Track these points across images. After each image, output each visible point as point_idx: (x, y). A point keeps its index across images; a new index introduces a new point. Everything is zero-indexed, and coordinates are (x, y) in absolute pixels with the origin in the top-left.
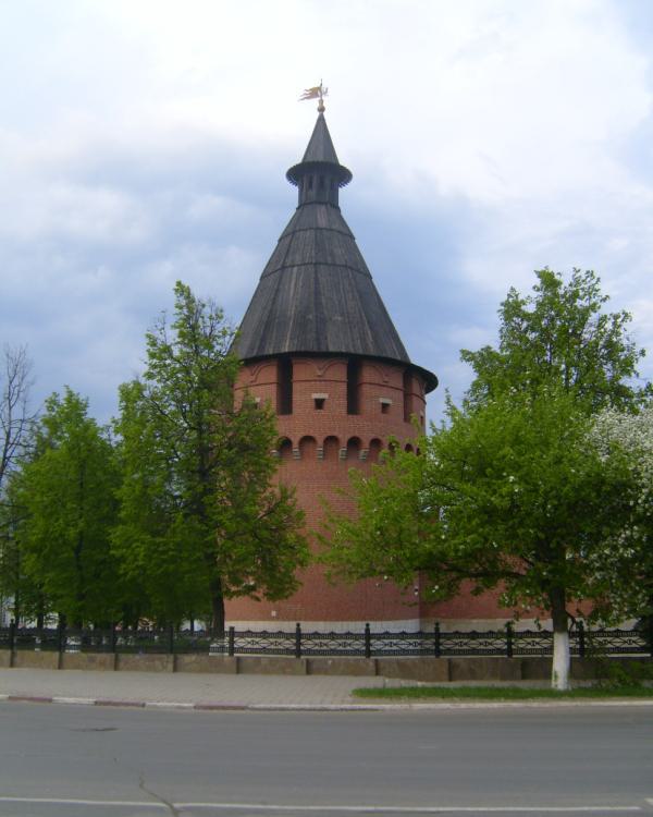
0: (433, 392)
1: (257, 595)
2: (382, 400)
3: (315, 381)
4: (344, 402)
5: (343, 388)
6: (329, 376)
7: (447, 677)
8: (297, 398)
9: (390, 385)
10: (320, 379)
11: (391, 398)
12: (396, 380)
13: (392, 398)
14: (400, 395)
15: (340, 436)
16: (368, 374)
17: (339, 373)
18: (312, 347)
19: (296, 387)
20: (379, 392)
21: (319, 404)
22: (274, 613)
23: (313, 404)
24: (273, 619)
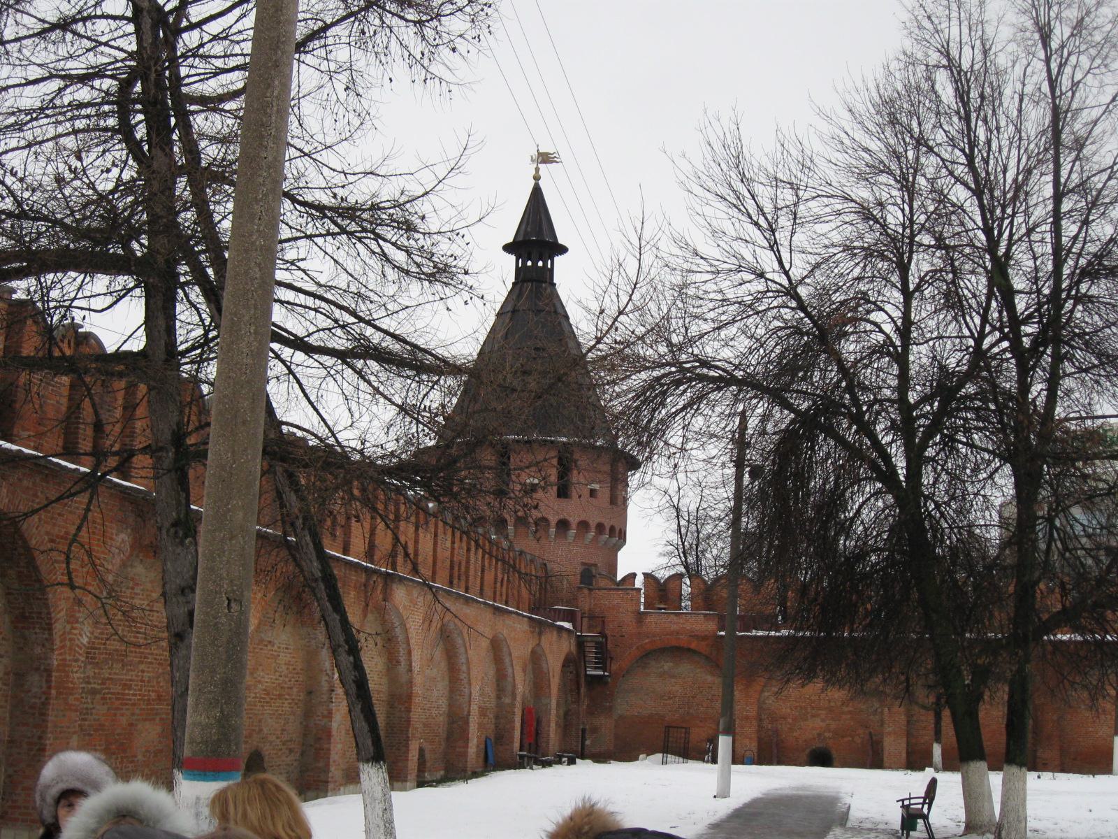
21: (593, 493)
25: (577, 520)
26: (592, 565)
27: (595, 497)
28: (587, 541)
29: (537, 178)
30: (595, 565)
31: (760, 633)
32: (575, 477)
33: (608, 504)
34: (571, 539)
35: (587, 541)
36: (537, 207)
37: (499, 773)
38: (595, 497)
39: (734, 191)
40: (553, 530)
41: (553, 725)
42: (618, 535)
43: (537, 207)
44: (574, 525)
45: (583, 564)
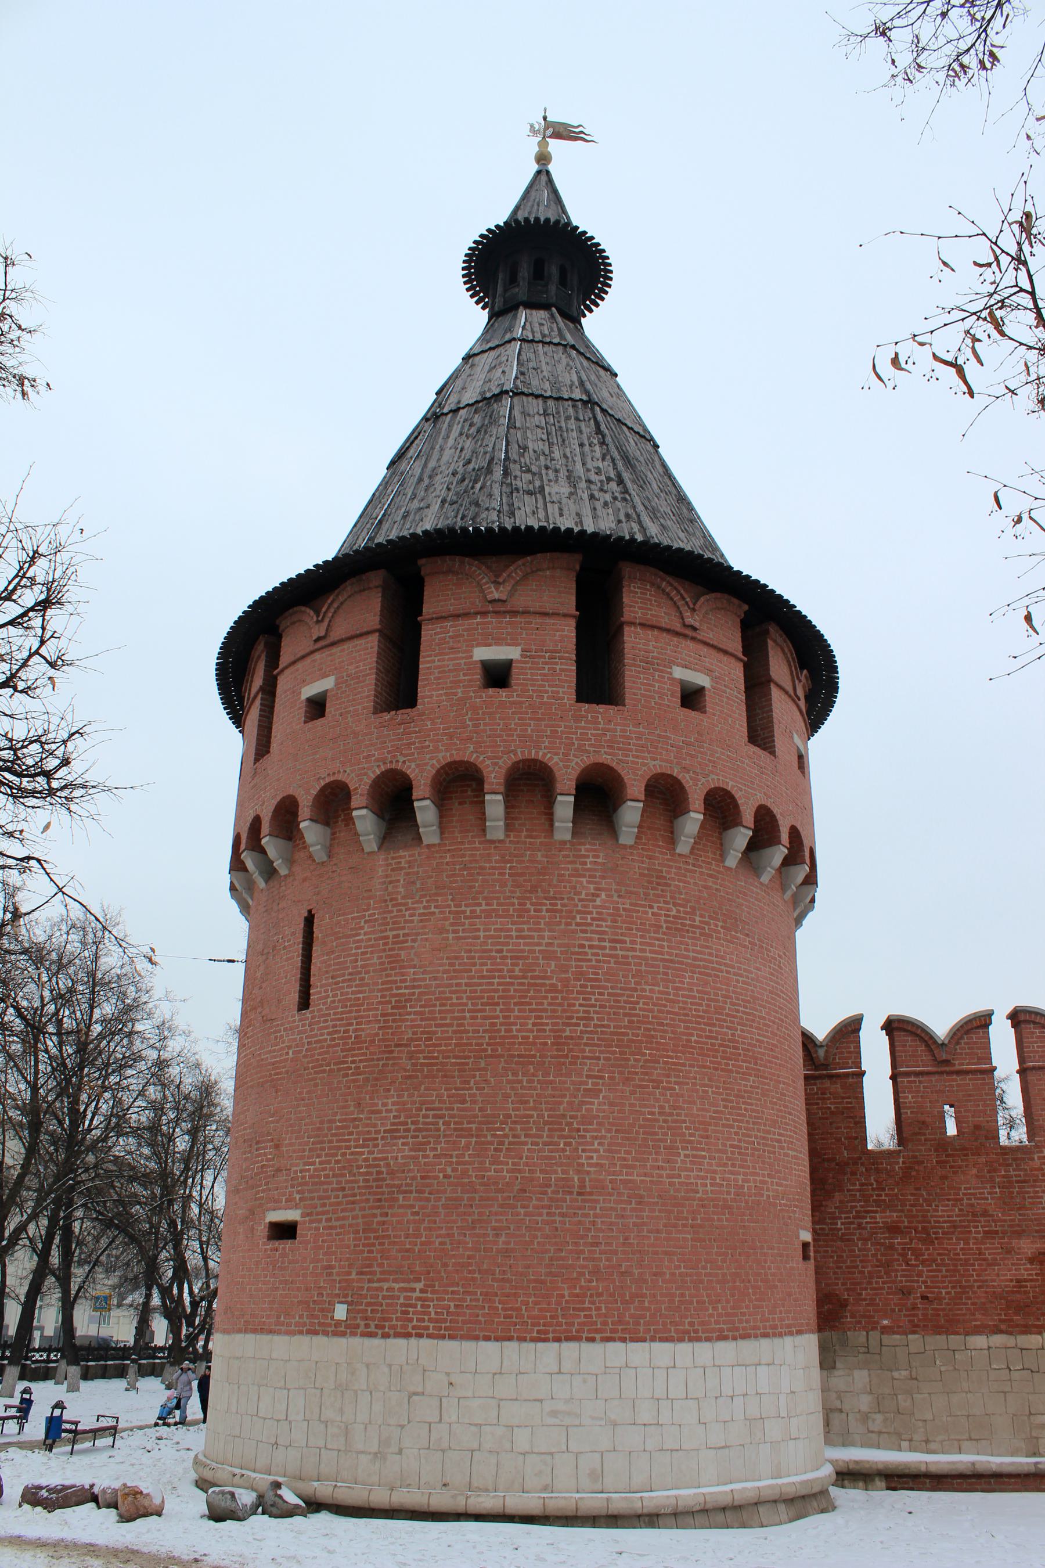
0: (216, 649)
1: (583, 428)
2: (484, 653)
3: (484, 614)
4: (567, 669)
5: (566, 633)
6: (525, 598)
7: (800, 1286)
8: (429, 662)
9: (701, 635)
10: (499, 609)
11: (709, 672)
12: (723, 628)
13: (720, 676)
14: (736, 672)
15: (554, 761)
16: (640, 601)
17: (555, 593)
18: (719, 1451)
19: (429, 634)
20: (673, 655)
21: (497, 676)
22: (341, 1312)
23: (478, 676)
24: (339, 1330)
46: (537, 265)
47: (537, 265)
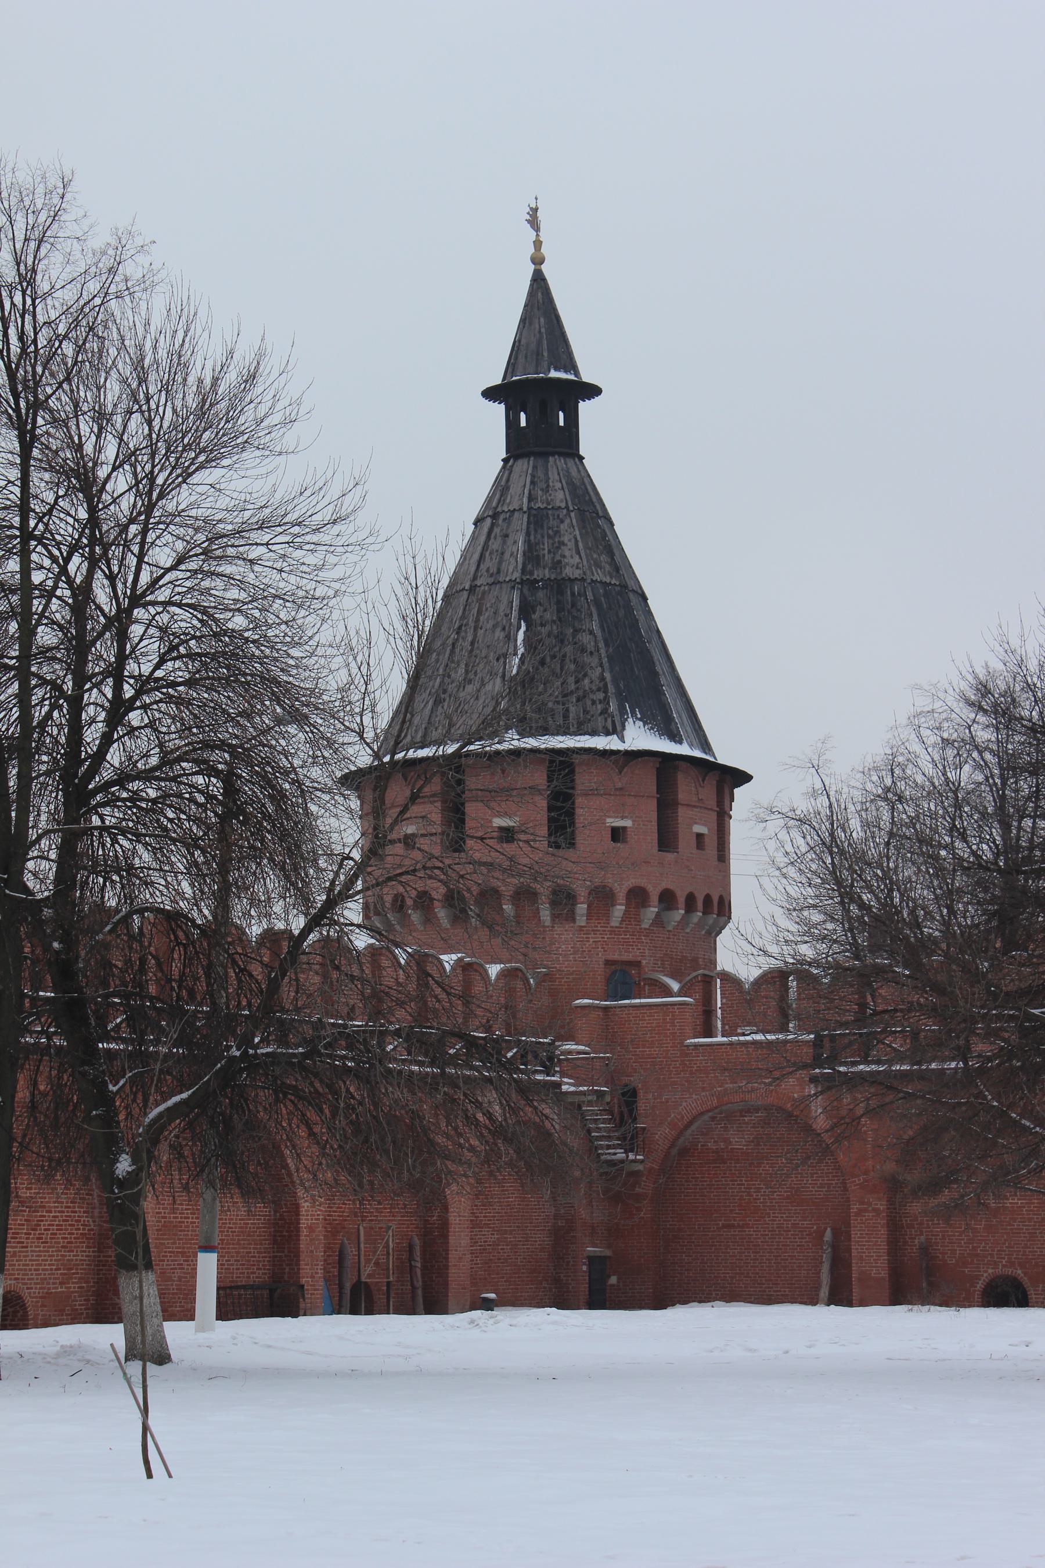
21: (617, 834)
25: (659, 889)
26: (630, 963)
27: (625, 841)
28: (615, 922)
29: (538, 260)
30: (637, 964)
31: (905, 1067)
32: (585, 810)
33: (695, 850)
34: (581, 921)
35: (615, 922)
36: (542, 320)
37: (510, 1308)
38: (625, 841)
39: (184, 341)
40: (582, 908)
41: (825, 1282)
42: (719, 908)
43: (542, 320)
44: (621, 896)
45: (608, 963)
46: (542, 398)
47: (542, 398)
